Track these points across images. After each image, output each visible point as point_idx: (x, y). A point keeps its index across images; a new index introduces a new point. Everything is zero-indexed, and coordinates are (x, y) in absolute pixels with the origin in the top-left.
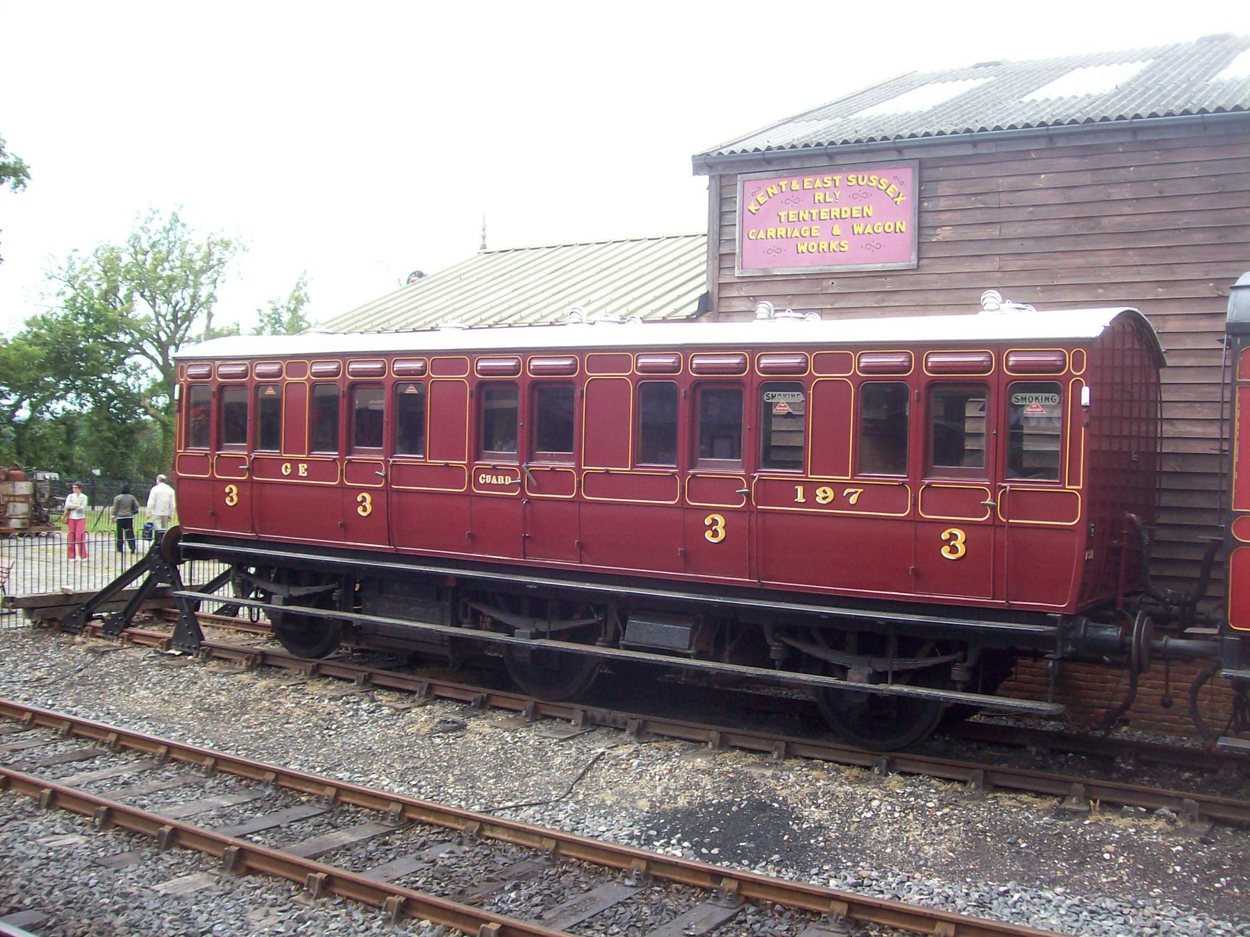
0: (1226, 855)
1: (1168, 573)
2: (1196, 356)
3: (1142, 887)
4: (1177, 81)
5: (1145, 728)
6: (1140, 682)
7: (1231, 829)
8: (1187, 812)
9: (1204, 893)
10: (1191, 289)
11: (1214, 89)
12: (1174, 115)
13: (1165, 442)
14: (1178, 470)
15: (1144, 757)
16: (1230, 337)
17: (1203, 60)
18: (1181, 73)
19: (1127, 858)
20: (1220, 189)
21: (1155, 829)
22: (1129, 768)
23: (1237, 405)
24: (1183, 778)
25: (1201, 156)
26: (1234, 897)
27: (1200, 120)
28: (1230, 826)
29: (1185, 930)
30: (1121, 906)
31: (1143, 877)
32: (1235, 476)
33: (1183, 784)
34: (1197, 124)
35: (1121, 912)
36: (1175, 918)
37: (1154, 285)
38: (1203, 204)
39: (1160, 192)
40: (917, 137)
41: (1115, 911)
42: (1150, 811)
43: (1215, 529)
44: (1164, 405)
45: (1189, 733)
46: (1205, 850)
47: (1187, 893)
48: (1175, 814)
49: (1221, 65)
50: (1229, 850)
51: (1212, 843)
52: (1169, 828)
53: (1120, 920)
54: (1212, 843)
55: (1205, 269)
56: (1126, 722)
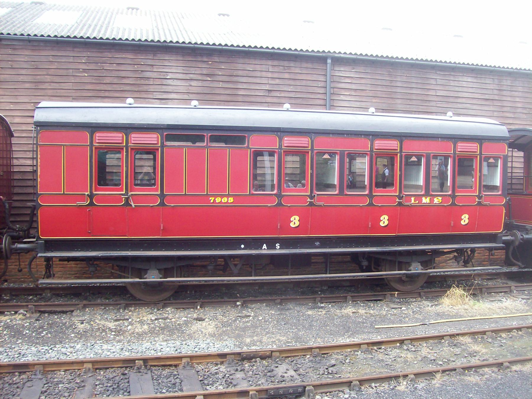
0: (45, 323)
1: (19, 220)
2: (26, 133)
3: (14, 340)
4: (20, 20)
5: (14, 282)
6: (9, 264)
7: (47, 314)
8: (30, 310)
9: (37, 338)
10: (25, 106)
11: (34, 26)
12: (17, 35)
13: (14, 167)
14: (21, 178)
15: (13, 293)
16: (35, 126)
17: (31, 12)
18: (22, 17)
19: (8, 331)
20: (35, 67)
21: (18, 319)
22: (8, 298)
23: (39, 153)
24: (29, 299)
25: (27, 53)
26: (49, 338)
27: (27, 39)
28: (47, 313)
29: (30, 353)
30: (5, 349)
31: (14, 337)
32: (39, 180)
33: (29, 301)
34: (26, 40)
35: (6, 351)
36: (27, 349)
37: (9, 103)
38: (29, 72)
39: (11, 66)
40: (4, 35)
41: (3, 351)
42: (16, 313)
43: (33, 201)
44: (13, 152)
45: (31, 282)
46: (37, 323)
47: (31, 340)
48: (25, 312)
49: (39, 15)
50: (46, 321)
51: (40, 320)
52: (24, 317)
53: (6, 354)
54: (40, 320)
55: (30, 98)
56: (6, 281)
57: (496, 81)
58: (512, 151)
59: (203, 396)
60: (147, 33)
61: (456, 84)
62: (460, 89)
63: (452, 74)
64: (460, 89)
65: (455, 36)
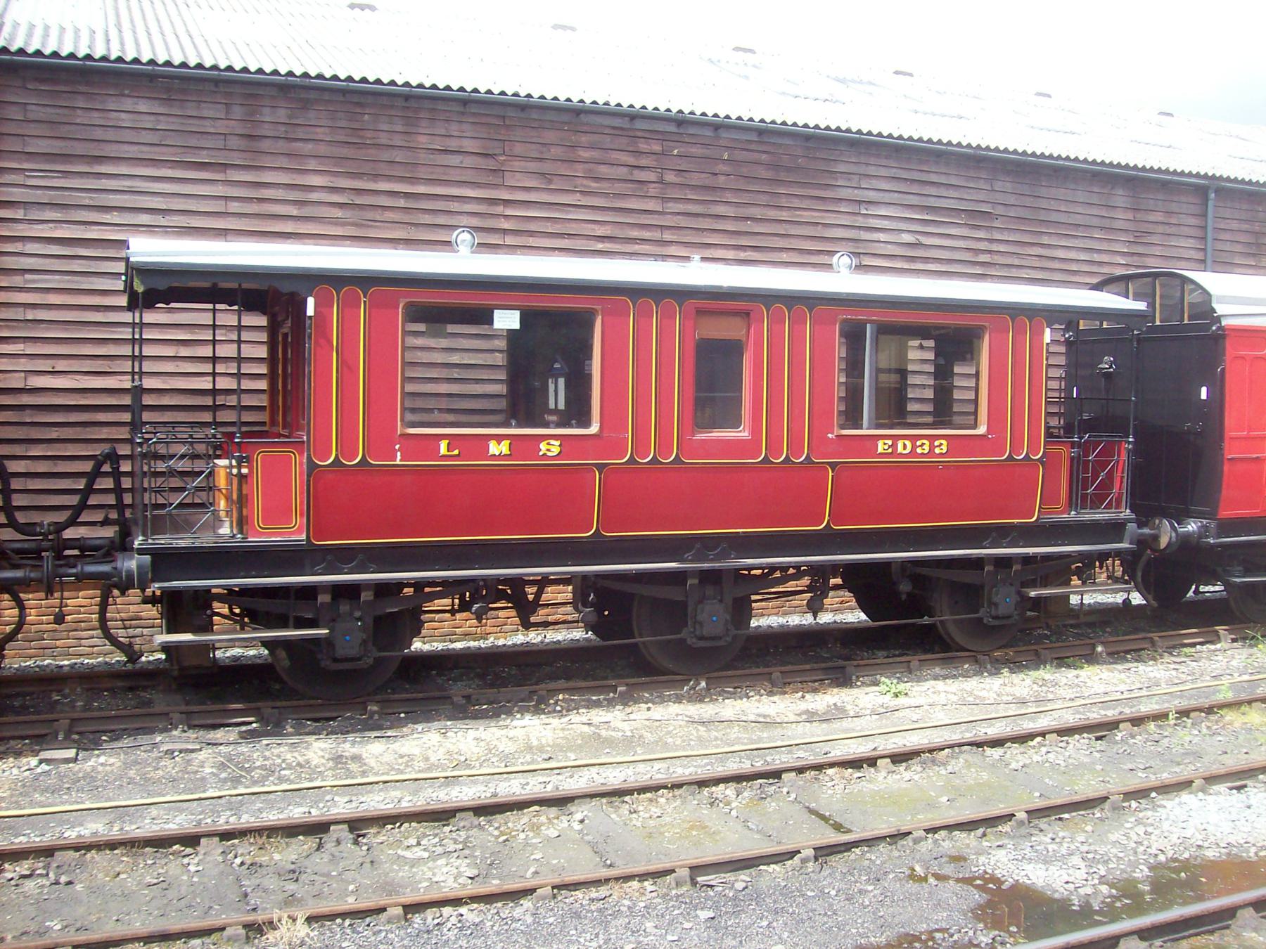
57: (238, 112)
58: (214, 310)
59: (401, 908)
60: (92, 39)
61: (96, 118)
62: (110, 135)
63: (82, 89)
64: (110, 135)
65: (897, 73)
